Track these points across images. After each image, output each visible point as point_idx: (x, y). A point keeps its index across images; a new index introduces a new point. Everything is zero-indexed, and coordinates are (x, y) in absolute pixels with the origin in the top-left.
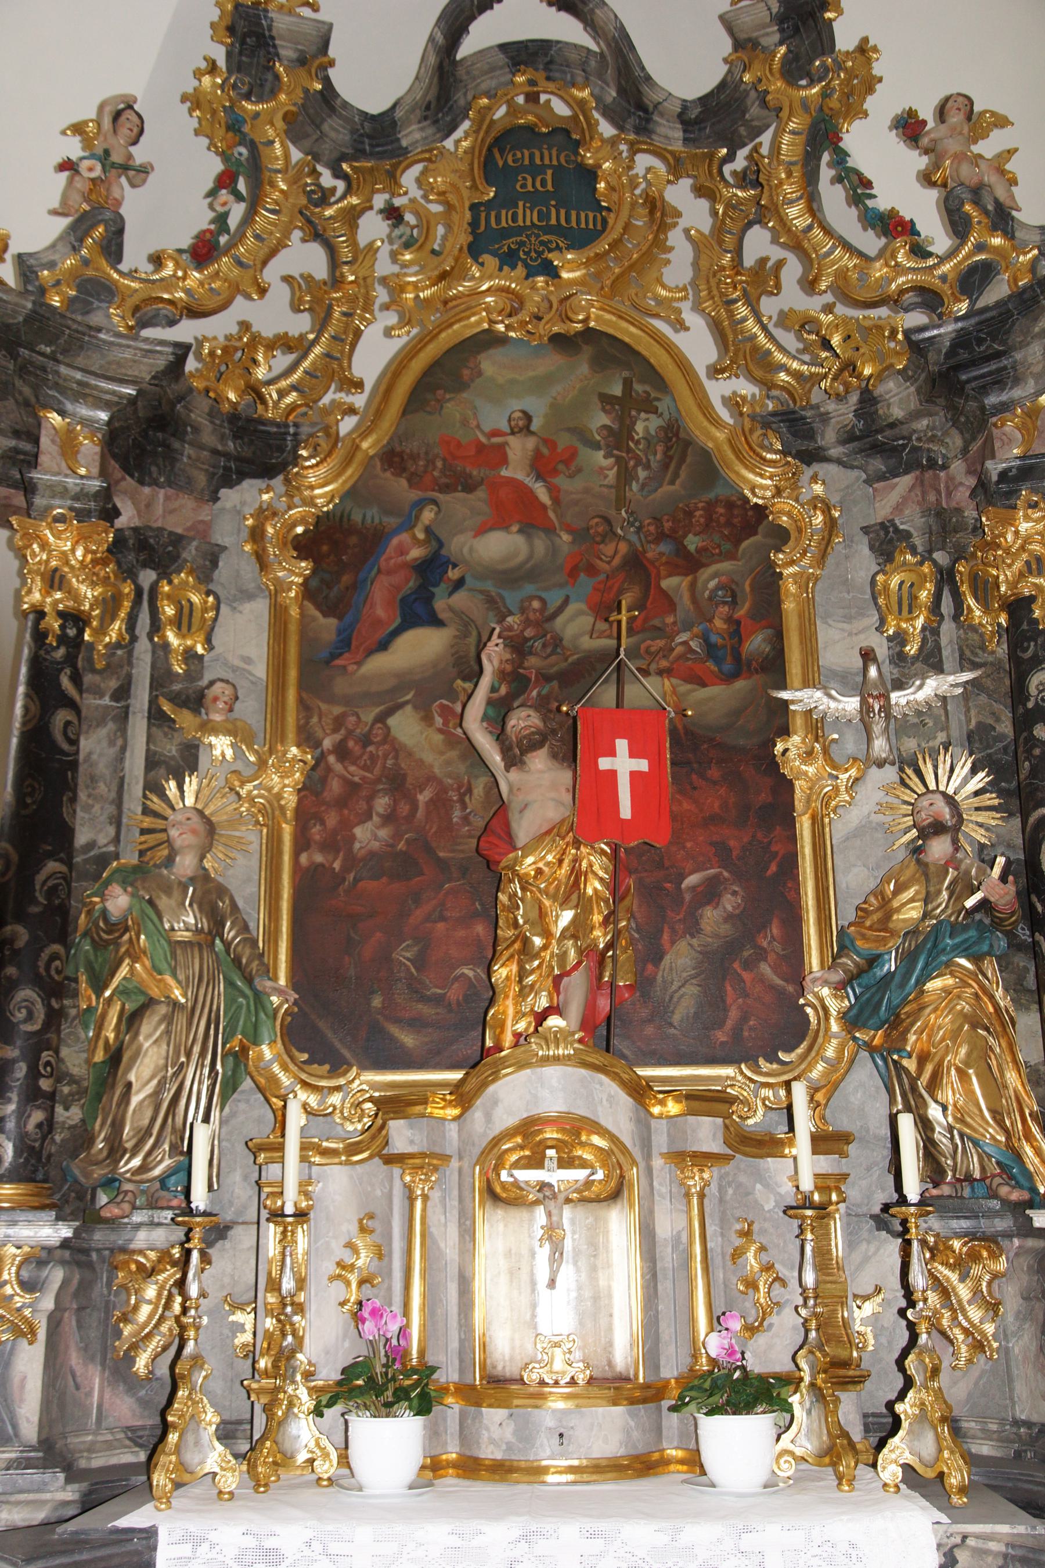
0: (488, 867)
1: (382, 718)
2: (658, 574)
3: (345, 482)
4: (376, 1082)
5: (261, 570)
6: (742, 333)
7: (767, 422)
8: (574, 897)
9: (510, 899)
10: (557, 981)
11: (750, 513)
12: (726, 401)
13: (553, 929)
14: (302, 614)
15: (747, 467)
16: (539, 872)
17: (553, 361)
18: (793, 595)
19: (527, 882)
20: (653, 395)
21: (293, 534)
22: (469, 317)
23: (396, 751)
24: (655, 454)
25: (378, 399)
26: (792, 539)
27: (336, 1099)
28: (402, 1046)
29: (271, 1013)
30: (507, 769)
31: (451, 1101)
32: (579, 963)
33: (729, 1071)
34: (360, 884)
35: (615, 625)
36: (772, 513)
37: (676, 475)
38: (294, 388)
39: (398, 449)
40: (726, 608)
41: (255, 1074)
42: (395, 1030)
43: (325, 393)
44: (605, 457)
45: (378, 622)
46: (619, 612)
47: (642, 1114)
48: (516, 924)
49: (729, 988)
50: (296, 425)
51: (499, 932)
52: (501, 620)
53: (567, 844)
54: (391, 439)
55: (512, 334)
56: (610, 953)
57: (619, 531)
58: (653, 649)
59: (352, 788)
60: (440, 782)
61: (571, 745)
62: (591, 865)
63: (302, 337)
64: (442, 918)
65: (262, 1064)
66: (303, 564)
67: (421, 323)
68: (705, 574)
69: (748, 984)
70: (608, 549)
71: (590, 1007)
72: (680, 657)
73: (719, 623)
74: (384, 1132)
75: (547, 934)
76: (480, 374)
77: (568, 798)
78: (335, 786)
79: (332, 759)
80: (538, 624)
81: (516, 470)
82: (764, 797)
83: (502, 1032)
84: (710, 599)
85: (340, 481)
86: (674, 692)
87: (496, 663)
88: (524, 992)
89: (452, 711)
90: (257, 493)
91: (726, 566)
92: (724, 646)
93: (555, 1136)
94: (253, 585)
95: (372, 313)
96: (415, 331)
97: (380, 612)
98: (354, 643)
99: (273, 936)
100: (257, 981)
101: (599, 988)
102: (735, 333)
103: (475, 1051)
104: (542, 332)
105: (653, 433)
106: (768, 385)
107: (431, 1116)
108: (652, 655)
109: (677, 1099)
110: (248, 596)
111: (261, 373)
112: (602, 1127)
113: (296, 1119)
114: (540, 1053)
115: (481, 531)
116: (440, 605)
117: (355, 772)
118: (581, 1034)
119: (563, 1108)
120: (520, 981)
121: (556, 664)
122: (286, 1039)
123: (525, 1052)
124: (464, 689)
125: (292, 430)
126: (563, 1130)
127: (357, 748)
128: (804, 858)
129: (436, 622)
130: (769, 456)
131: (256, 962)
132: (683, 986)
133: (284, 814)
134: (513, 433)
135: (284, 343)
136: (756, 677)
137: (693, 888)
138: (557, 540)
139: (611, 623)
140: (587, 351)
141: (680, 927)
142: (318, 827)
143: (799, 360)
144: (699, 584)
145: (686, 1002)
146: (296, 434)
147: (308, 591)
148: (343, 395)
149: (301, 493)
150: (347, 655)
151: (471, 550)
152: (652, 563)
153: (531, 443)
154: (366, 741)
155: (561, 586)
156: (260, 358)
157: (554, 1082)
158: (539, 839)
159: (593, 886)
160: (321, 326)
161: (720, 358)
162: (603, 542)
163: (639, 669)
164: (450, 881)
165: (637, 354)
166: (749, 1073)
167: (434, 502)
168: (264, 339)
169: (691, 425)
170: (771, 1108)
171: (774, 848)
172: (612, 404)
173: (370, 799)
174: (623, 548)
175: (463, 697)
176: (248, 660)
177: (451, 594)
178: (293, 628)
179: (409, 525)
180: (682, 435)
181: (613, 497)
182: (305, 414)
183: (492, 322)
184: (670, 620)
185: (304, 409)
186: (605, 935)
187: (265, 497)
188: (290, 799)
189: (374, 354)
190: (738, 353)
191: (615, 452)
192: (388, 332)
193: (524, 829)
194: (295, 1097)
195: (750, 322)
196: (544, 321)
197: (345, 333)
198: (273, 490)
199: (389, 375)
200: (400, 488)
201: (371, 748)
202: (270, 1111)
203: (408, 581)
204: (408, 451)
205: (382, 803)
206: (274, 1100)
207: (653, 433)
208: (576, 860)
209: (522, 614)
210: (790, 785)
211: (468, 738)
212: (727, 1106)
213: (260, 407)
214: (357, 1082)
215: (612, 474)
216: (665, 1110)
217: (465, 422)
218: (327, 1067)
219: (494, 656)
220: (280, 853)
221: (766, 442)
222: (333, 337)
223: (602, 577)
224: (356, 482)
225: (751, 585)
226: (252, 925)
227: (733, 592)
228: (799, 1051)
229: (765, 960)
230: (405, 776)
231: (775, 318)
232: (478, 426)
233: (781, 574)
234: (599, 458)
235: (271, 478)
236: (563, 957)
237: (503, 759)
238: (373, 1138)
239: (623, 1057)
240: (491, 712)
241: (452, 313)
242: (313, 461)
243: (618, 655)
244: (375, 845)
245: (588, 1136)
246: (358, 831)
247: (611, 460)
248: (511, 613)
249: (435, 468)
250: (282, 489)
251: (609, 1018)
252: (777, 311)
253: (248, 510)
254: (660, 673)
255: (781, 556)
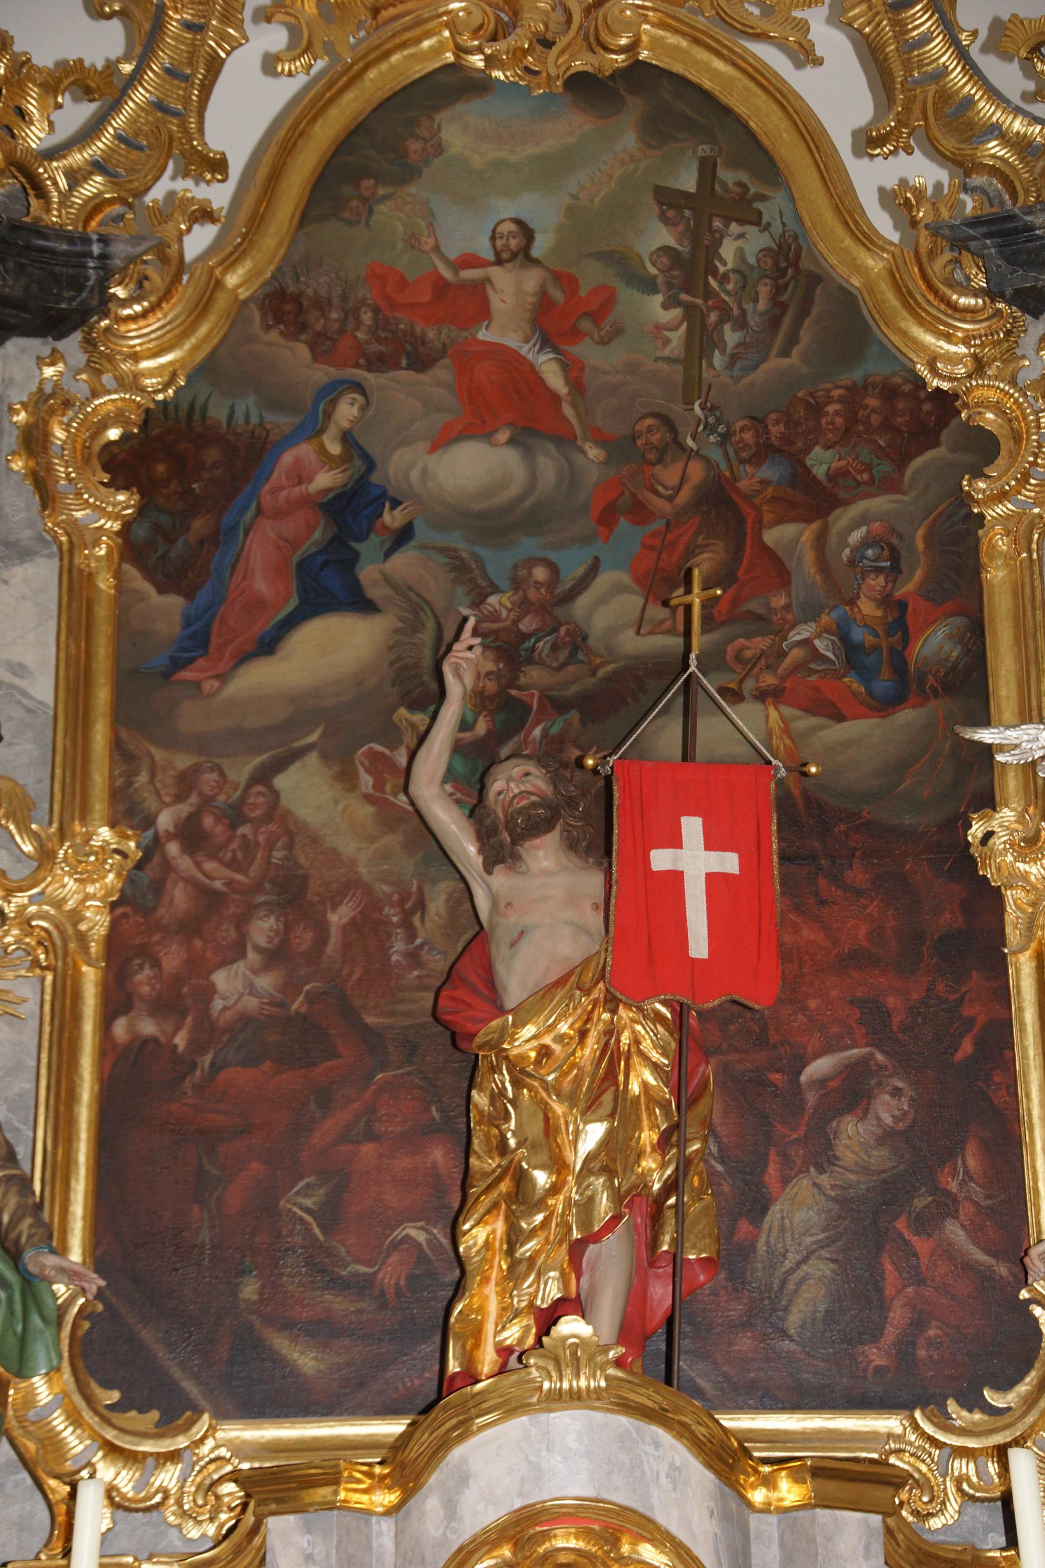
0: (454, 1044)
1: (264, 776)
2: (759, 519)
3: (195, 348)
4: (244, 1442)
5: (44, 507)
6: (920, 66)
7: (959, 238)
8: (608, 1098)
9: (492, 1101)
10: (577, 1250)
11: (927, 407)
12: (887, 198)
13: (569, 1156)
14: (119, 588)
15: (921, 322)
16: (545, 1052)
17: (572, 126)
18: (1005, 555)
19: (523, 1071)
20: (753, 190)
21: (101, 441)
22: (418, 41)
23: (291, 834)
24: (756, 301)
25: (253, 195)
26: (1004, 453)
27: (168, 1477)
28: (295, 1373)
29: (53, 1315)
30: (488, 868)
31: (382, 1478)
32: (616, 1219)
33: (891, 1423)
34: (224, 1075)
35: (681, 612)
36: (966, 405)
37: (793, 339)
38: (97, 166)
39: (292, 289)
40: (881, 580)
41: (17, 1433)
42: (281, 1343)
43: (157, 179)
44: (665, 306)
45: (260, 604)
46: (689, 591)
47: (733, 1504)
48: (503, 1148)
49: (889, 1267)
50: (104, 240)
51: (473, 1161)
52: (478, 600)
53: (595, 1003)
54: (279, 269)
55: (498, 74)
56: (672, 1201)
57: (690, 442)
58: (749, 654)
59: (209, 901)
60: (368, 890)
61: (602, 826)
62: (636, 1041)
63: (111, 66)
64: (371, 1135)
65: (31, 1414)
66: (121, 498)
67: (329, 49)
68: (841, 518)
69: (924, 1260)
70: (669, 474)
71: (636, 1298)
72: (799, 667)
73: (867, 607)
74: (257, 1540)
75: (558, 1165)
76: (440, 149)
77: (596, 921)
78: (179, 897)
79: (173, 848)
80: (543, 609)
81: (505, 330)
82: (949, 920)
83: (477, 1345)
84: (852, 563)
85: (187, 346)
86: (786, 730)
87: (469, 680)
88: (514, 1274)
89: (390, 763)
90: (33, 363)
91: (881, 503)
92: (877, 648)
93: (573, 1544)
94: (27, 533)
95: (239, 26)
96: (320, 65)
97: (262, 586)
98: (214, 641)
99: (60, 1171)
100: (28, 1256)
101: (652, 1264)
102: (907, 66)
103: (426, 1382)
104: (553, 71)
105: (752, 260)
106: (964, 165)
107: (345, 1507)
108: (748, 665)
109: (797, 1477)
110: (23, 554)
111: (35, 136)
112: (658, 1527)
113: (92, 1518)
114: (546, 1385)
115: (442, 441)
116: (368, 573)
117: (216, 874)
118: (621, 1350)
119: (588, 1492)
120: (510, 1252)
121: (576, 681)
122: (80, 1365)
123: (518, 1382)
124: (412, 725)
125: (96, 249)
126: (586, 1534)
127: (219, 829)
128: (1022, 1030)
129: (361, 604)
130: (963, 301)
131: (28, 1221)
132: (805, 1260)
133: (85, 948)
134: (499, 262)
135: (72, 79)
136: (933, 703)
137: (821, 1083)
138: (578, 458)
139: (674, 610)
140: (635, 107)
141: (798, 1154)
142: (147, 971)
143: (1025, 114)
144: (833, 538)
145: (810, 1294)
146: (103, 257)
147: (131, 547)
148: (189, 183)
149: (116, 367)
150: (201, 662)
151: (425, 473)
152: (747, 498)
153: (532, 280)
154: (235, 816)
155: (586, 540)
156: (32, 107)
157: (571, 1441)
158: (544, 995)
159: (641, 1079)
160: (146, 44)
161: (879, 116)
162: (660, 461)
163: (723, 691)
164: (384, 1066)
165: (727, 111)
166: (929, 1429)
167: (358, 387)
168: (39, 70)
169: (821, 246)
170: (973, 1499)
171: (967, 1012)
172: (679, 208)
173: (242, 921)
174: (696, 472)
175: (410, 739)
176: (19, 669)
177: (388, 554)
178: (103, 612)
179: (313, 427)
180: (805, 264)
181: (679, 379)
182: (121, 217)
183: (461, 50)
184: (779, 601)
185: (117, 209)
186: (663, 1166)
187: (49, 372)
188: (97, 922)
189: (243, 109)
190: (912, 106)
191: (684, 297)
192: (270, 65)
193: (517, 975)
194: (92, 1476)
195: (937, 45)
196: (556, 49)
197: (190, 63)
198: (62, 358)
199: (273, 149)
200: (297, 362)
201: (245, 830)
202: (42, 1505)
203: (311, 529)
204: (310, 292)
205: (263, 929)
206: (53, 1483)
207: (752, 260)
208: (611, 1032)
209: (516, 590)
210: (996, 897)
211: (418, 812)
212: (890, 1490)
213: (34, 202)
214: (210, 1443)
215: (677, 337)
216: (774, 1495)
217: (412, 241)
218: (154, 1415)
219: (465, 667)
220: (77, 1018)
221: (958, 276)
222: (167, 71)
223: (659, 524)
224: (216, 348)
225: (926, 538)
226: (22, 1152)
227: (893, 550)
228: (1023, 1388)
229: (954, 1215)
230: (305, 879)
231: (983, 35)
232: (437, 249)
233: (981, 516)
234: (655, 308)
235: (59, 337)
236: (587, 1206)
237: (481, 851)
238: (238, 1551)
239: (697, 1393)
240: (459, 766)
241: (389, 30)
242: (137, 308)
243: (686, 666)
244: (251, 1003)
245: (634, 1544)
246: (220, 979)
247: (676, 313)
248: (495, 590)
249: (359, 323)
250: (82, 358)
251: (670, 1321)
252: (988, 21)
253: (18, 396)
254: (762, 696)
255: (982, 485)
